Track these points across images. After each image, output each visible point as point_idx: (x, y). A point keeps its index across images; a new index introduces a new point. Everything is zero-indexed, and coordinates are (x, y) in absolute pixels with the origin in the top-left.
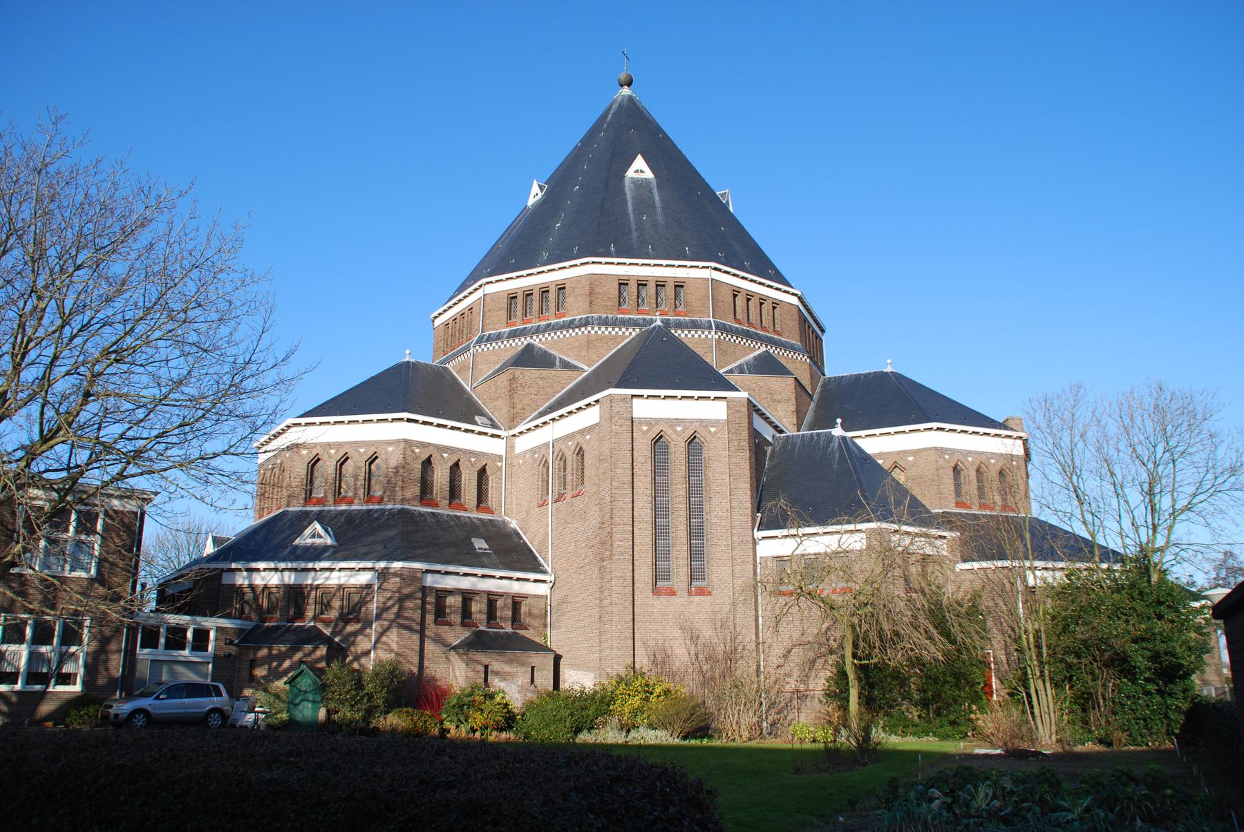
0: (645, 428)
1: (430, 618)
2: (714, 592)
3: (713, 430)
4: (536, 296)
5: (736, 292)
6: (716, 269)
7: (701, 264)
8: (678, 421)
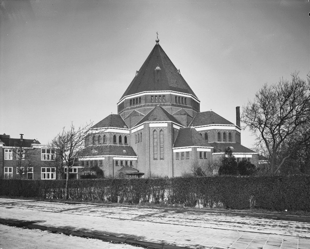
0: (152, 129)
1: (115, 165)
2: (165, 159)
3: (165, 129)
4: (135, 100)
5: (176, 97)
6: (171, 92)
7: (168, 91)
8: (158, 127)
